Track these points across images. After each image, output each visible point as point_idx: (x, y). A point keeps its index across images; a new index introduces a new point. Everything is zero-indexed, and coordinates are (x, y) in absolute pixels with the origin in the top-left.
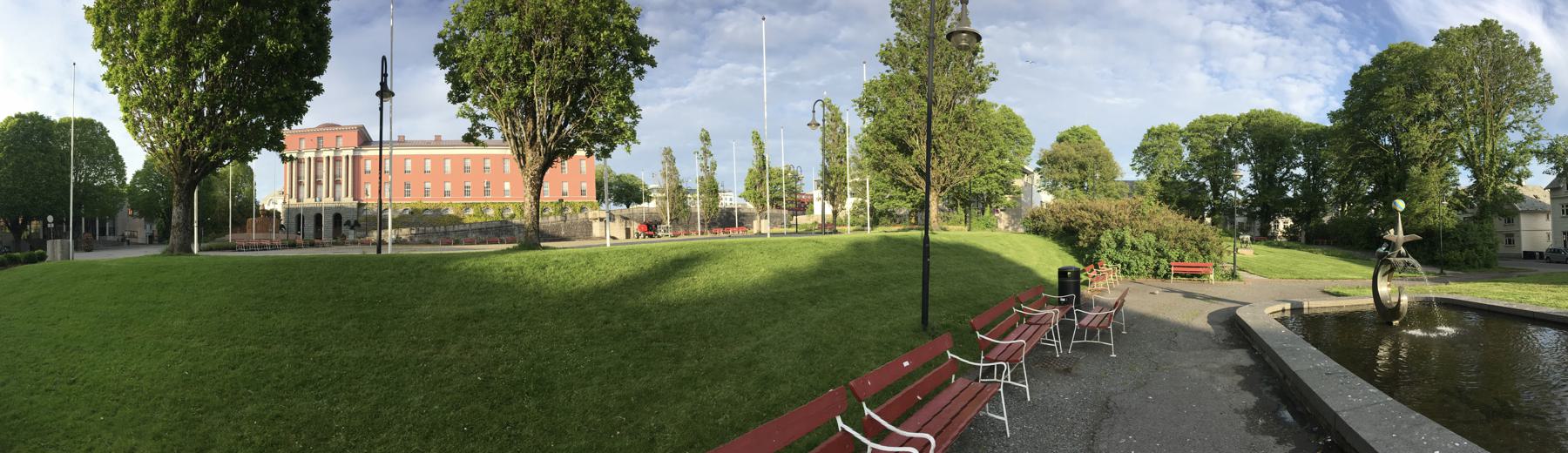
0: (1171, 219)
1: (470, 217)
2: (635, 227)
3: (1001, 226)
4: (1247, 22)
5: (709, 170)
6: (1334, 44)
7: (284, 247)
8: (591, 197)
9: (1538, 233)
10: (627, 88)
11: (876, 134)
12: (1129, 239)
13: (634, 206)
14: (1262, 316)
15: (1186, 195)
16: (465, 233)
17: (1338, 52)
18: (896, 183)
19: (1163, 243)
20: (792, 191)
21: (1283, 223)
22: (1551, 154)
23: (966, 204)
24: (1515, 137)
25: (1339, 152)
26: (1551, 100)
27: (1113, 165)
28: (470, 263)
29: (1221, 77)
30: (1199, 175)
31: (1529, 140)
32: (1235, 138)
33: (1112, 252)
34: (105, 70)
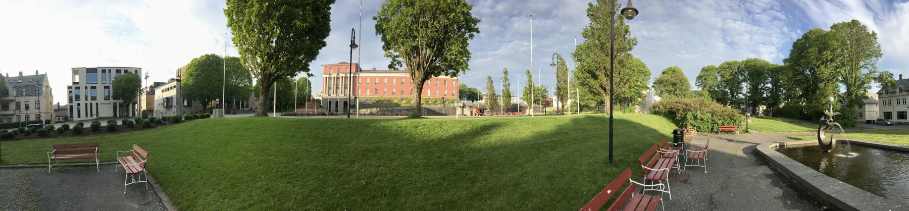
0: (718, 107)
1: (404, 104)
2: (474, 111)
3: (636, 111)
4: (742, 20)
5: (507, 86)
6: (781, 29)
7: (319, 115)
8: (456, 97)
9: (873, 112)
10: (464, 42)
11: (582, 70)
12: (699, 115)
13: (475, 102)
14: (769, 149)
15: (719, 96)
16: (401, 111)
17: (783, 33)
18: (591, 92)
19: (715, 118)
20: (544, 97)
21: (762, 108)
22: (880, 79)
23: (621, 102)
24: (864, 71)
25: (788, 77)
26: (881, 55)
27: (688, 84)
28: (382, 124)
29: (731, 45)
30: (725, 88)
31: (871, 73)
32: (740, 71)
33: (692, 121)
34: (233, 36)
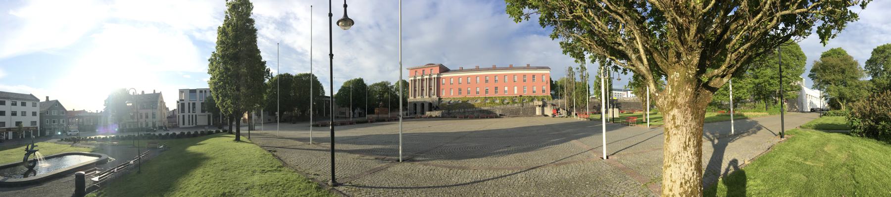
16: (473, 112)
